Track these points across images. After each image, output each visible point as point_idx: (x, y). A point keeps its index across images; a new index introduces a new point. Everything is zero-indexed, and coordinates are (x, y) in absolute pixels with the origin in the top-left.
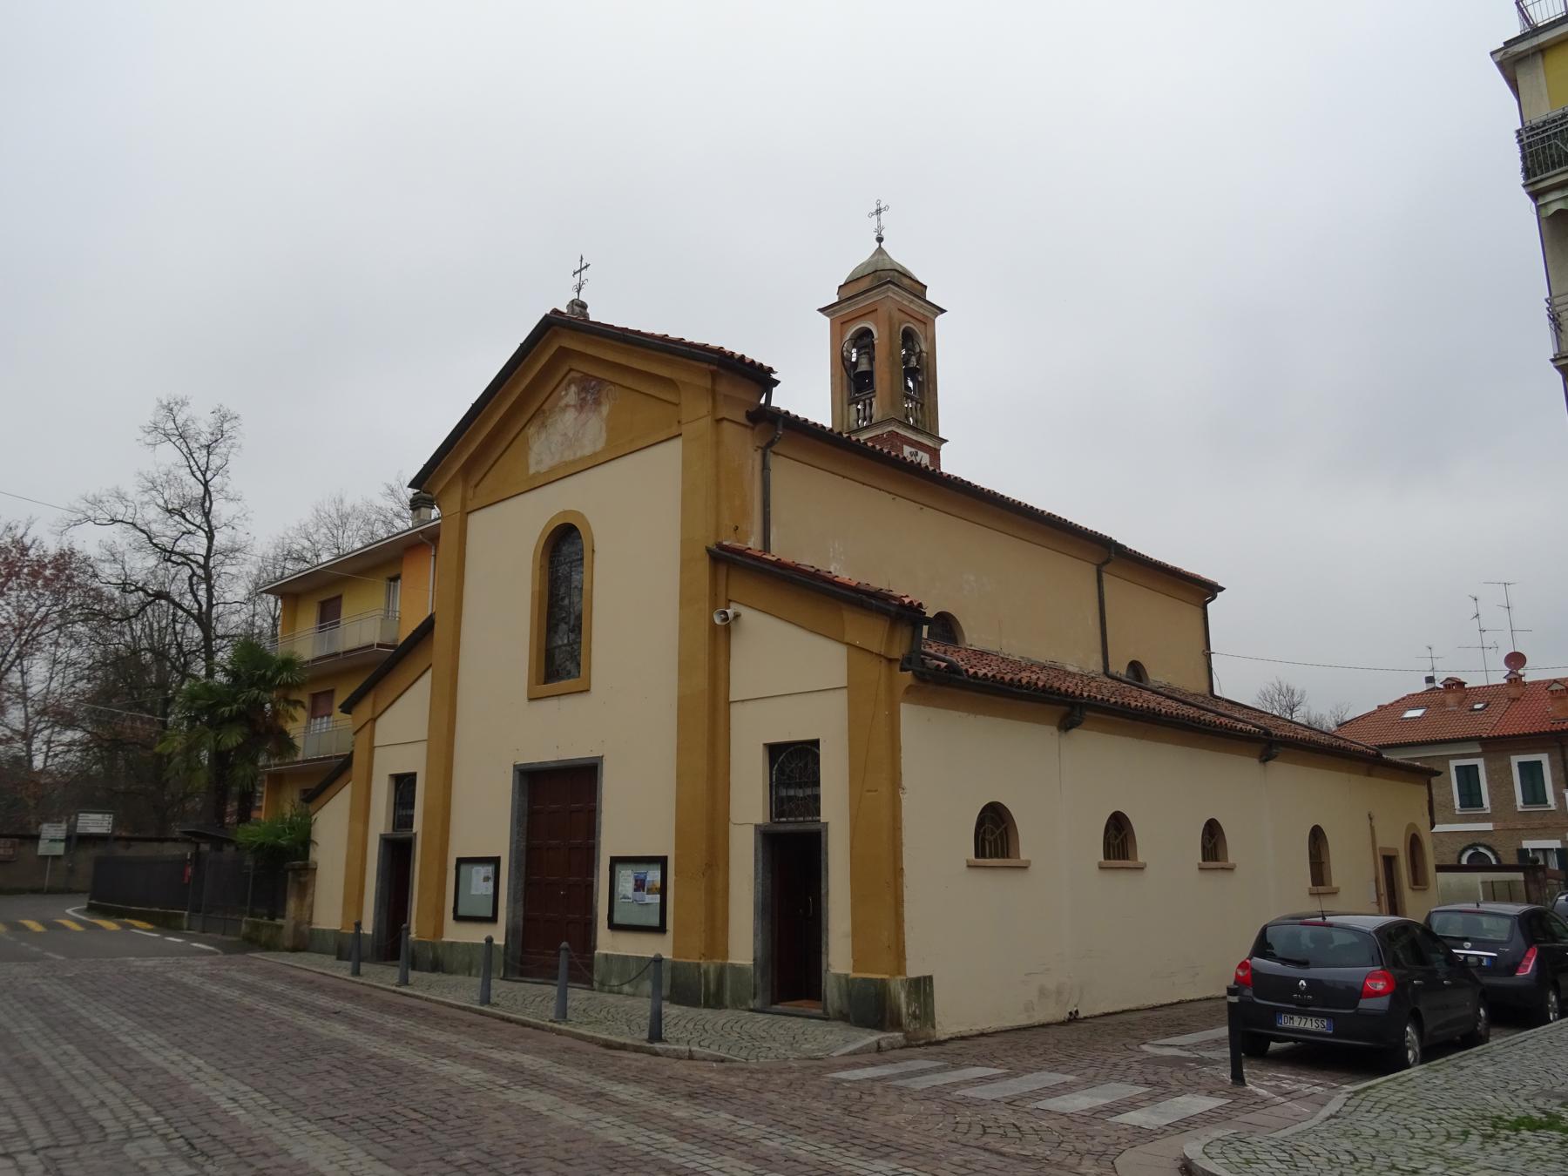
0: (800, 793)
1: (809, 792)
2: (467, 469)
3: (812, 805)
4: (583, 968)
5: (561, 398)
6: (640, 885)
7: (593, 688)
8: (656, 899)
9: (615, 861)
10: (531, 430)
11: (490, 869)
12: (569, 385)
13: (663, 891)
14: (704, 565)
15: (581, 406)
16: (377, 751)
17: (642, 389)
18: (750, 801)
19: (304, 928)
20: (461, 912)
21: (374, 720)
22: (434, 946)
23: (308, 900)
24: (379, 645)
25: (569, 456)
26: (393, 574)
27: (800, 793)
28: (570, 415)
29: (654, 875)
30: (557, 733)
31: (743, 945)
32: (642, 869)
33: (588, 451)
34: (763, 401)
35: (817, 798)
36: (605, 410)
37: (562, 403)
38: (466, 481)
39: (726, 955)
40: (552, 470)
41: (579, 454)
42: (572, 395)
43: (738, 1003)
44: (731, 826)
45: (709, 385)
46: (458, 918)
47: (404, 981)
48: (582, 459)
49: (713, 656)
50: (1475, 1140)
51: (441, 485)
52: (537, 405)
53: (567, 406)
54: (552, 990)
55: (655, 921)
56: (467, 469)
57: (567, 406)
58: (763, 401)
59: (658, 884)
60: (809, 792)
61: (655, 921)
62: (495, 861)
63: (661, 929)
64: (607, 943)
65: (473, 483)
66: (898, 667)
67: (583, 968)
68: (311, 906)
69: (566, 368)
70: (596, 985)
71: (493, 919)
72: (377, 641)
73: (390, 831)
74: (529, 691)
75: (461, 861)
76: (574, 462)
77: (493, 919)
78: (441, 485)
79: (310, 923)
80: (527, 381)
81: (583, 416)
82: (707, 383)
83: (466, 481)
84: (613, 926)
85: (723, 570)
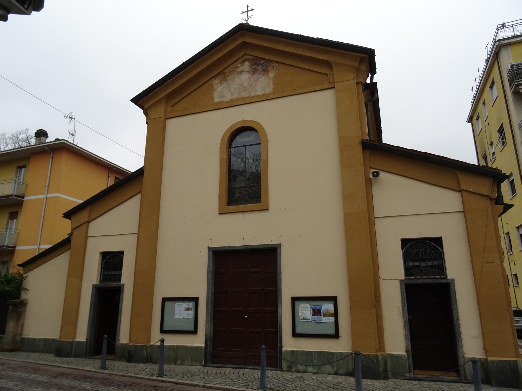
0: (423, 264)
1: (117, 273)
2: (169, 97)
3: (118, 278)
4: (275, 359)
5: (237, 67)
6: (317, 312)
7: (271, 208)
8: (332, 319)
9: (295, 300)
10: (215, 81)
11: (191, 304)
12: (244, 61)
13: (336, 314)
14: (358, 151)
15: (254, 72)
16: (89, 240)
18: (392, 269)
19: (18, 338)
20: (166, 328)
21: (89, 222)
22: (147, 348)
23: (21, 321)
24: (16, 196)
26: (20, 165)
27: (423, 264)
28: (245, 77)
29: (328, 307)
30: (244, 230)
31: (396, 341)
32: (317, 304)
33: (260, 93)
34: (368, 81)
35: (120, 275)
36: (272, 75)
37: (239, 70)
38: (167, 103)
39: (384, 351)
40: (231, 101)
41: (253, 94)
42: (246, 66)
43: (397, 375)
44: (381, 281)
45: (357, 65)
46: (295, 335)
47: (103, 367)
48: (257, 96)
49: (367, 195)
50: (197, 371)
51: (150, 103)
52: (221, 69)
53: (242, 71)
54: (257, 373)
55: (332, 332)
56: (169, 97)
57: (242, 71)
58: (368, 81)
60: (117, 273)
61: (332, 332)
62: (196, 300)
63: (336, 336)
64: (289, 344)
65: (172, 104)
66: (494, 202)
67: (275, 359)
68: (22, 326)
69: (244, 53)
70: (285, 365)
71: (195, 332)
72: (15, 193)
73: (98, 283)
74: (220, 209)
75: (165, 300)
77: (195, 332)
79: (21, 335)
80: (219, 56)
81: (255, 77)
82: (357, 65)
83: (167, 103)
84: (295, 335)
85: (368, 153)
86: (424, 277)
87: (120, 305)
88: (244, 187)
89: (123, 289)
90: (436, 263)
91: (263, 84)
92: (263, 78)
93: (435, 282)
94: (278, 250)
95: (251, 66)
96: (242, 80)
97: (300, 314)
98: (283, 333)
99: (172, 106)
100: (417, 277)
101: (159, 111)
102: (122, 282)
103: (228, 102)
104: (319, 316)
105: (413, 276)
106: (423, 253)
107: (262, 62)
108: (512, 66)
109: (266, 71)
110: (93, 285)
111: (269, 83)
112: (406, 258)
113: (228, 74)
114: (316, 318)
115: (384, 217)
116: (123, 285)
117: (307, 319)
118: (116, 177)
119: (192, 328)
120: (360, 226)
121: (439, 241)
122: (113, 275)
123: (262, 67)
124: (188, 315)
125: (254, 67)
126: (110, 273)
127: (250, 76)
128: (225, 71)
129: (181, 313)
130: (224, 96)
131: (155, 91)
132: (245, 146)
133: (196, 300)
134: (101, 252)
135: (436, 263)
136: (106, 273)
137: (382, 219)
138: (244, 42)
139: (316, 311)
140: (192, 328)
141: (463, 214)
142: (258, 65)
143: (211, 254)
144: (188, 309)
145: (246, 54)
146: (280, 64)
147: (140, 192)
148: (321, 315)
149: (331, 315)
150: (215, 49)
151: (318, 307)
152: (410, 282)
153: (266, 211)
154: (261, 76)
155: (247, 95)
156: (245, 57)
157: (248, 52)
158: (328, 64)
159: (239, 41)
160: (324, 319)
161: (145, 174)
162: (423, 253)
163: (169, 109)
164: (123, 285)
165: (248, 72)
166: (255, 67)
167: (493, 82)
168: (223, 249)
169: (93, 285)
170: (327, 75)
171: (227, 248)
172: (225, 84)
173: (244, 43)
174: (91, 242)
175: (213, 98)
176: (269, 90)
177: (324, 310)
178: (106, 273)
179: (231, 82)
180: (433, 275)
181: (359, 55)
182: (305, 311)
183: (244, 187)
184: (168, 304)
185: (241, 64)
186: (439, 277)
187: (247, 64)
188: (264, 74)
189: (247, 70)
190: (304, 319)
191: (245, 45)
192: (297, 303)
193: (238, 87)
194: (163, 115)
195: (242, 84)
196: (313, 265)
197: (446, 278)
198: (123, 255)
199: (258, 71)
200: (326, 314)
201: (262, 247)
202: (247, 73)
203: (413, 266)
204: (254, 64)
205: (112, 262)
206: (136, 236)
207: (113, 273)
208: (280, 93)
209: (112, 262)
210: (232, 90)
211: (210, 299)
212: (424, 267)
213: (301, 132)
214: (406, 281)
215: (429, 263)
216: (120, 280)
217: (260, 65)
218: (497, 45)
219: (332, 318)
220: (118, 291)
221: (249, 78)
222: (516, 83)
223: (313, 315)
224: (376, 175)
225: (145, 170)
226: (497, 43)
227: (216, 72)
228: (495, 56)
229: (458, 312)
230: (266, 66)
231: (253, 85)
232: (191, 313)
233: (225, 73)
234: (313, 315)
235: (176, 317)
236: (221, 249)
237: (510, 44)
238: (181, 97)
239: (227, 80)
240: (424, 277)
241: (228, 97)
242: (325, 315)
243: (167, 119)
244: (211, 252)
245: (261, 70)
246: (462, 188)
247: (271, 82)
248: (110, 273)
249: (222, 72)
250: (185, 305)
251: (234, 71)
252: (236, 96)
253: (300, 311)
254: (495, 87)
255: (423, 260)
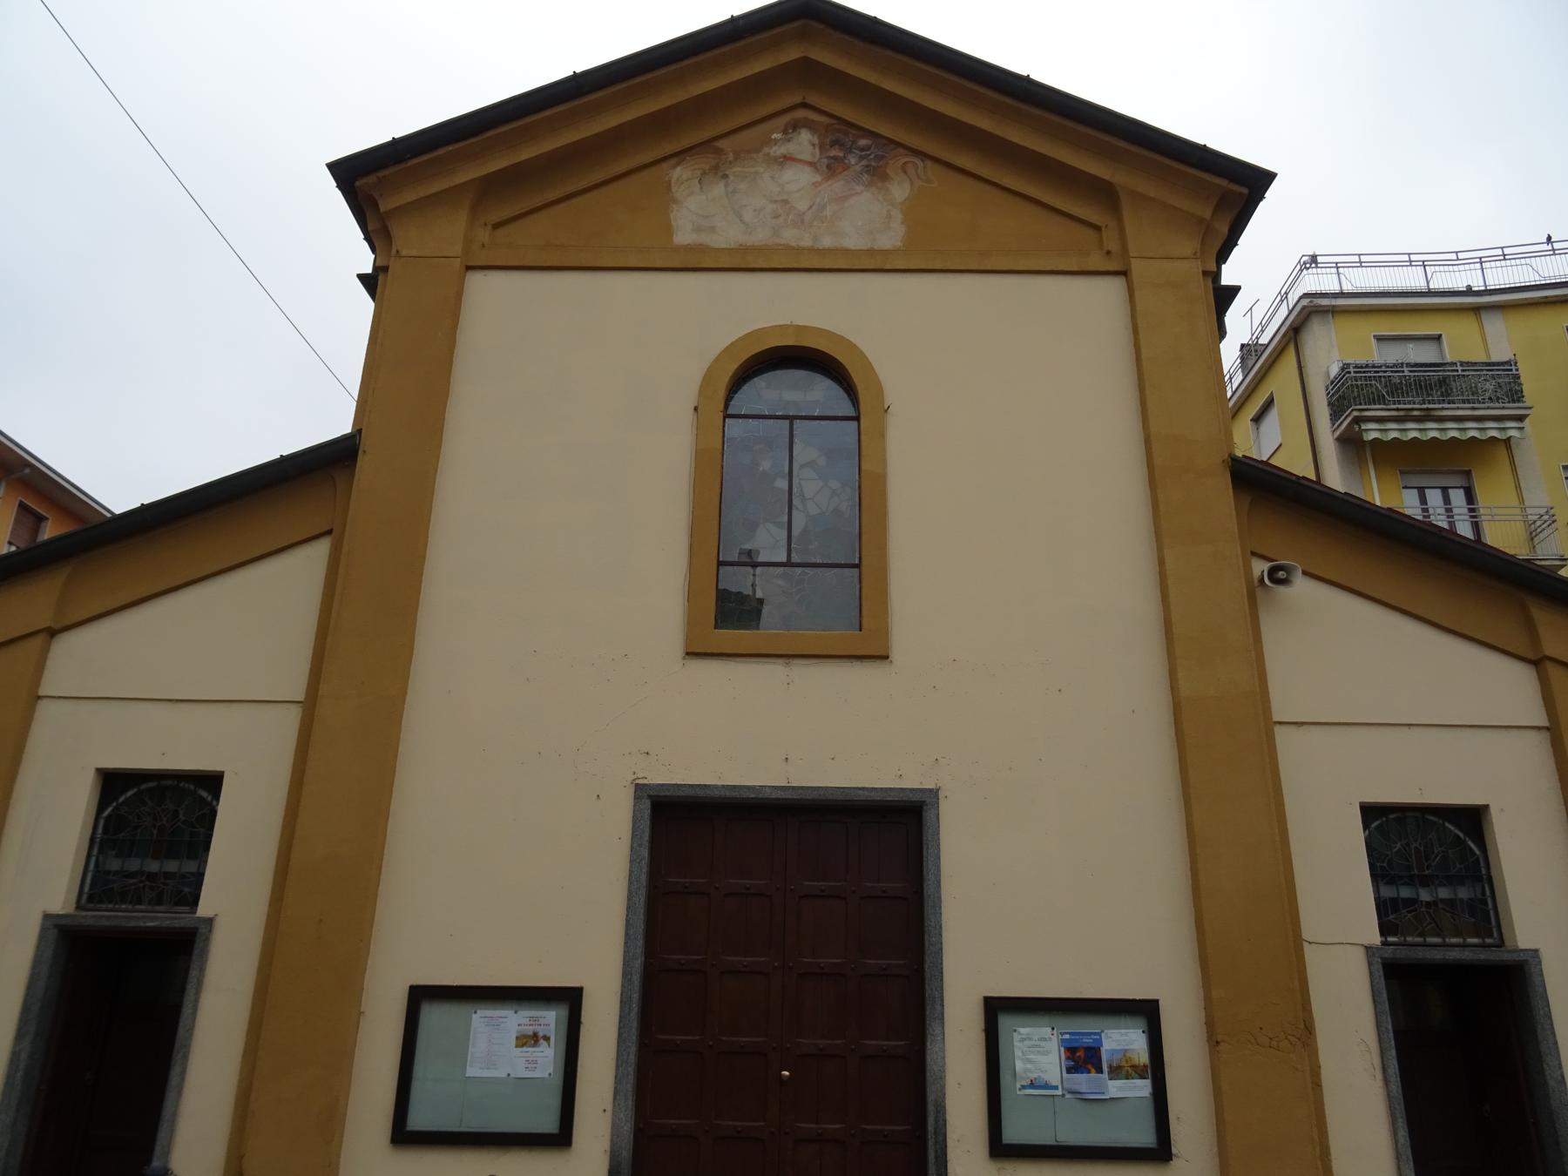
0: (1425, 895)
5: (770, 142)
6: (1083, 1058)
7: (896, 653)
10: (679, 172)
11: (550, 1019)
12: (795, 126)
13: (1156, 1069)
15: (833, 168)
16: (45, 710)
17: (1008, 181)
18: (1339, 909)
20: (419, 1120)
21: (52, 633)
25: (790, 236)
27: (1425, 895)
28: (798, 180)
29: (1125, 1039)
30: (781, 732)
32: (1084, 1026)
35: (199, 877)
36: (900, 190)
40: (744, 250)
41: (827, 242)
42: (804, 143)
51: (409, 196)
55: (1144, 1136)
57: (787, 159)
59: (1143, 1057)
61: (1144, 1136)
62: (570, 998)
69: (797, 99)
76: (799, 250)
78: (409, 196)
81: (838, 186)
82: (1207, 214)
86: (1431, 940)
87: (186, 1011)
88: (782, 566)
89: (207, 940)
90: (1463, 893)
91: (868, 213)
92: (867, 195)
93: (1482, 957)
94: (928, 815)
95: (822, 147)
96: (781, 186)
97: (1019, 1065)
98: (950, 1143)
99: (496, 226)
100: (1409, 939)
101: (445, 233)
102: (203, 910)
103: (730, 251)
104: (1093, 1075)
105: (1395, 934)
106: (1433, 855)
107: (863, 142)
108: (1345, 368)
109: (876, 174)
110: (47, 917)
111: (889, 216)
112: (1381, 872)
113: (731, 157)
114: (1082, 1081)
115: (1303, 724)
116: (209, 922)
117: (1047, 1086)
118: (22, 506)
119: (548, 1123)
120: (1223, 748)
121: (1473, 819)
122: (152, 877)
123: (862, 158)
124: (532, 1064)
125: (832, 154)
126: (134, 865)
127: (818, 178)
128: (720, 144)
129: (499, 1057)
130: (713, 229)
131: (441, 151)
132: (791, 419)
133: (570, 998)
134: (99, 771)
135: (1463, 893)
136: (114, 865)
137: (1293, 728)
138: (805, 58)
139: (1080, 1054)
140: (550, 1125)
141: (1545, 736)
142: (850, 151)
143: (647, 813)
144: (530, 1039)
145: (804, 105)
146: (929, 163)
147: (329, 532)
148: (1100, 1070)
149: (1140, 1072)
150: (701, 57)
151: (1088, 1041)
152: (1403, 954)
153: (878, 663)
154: (859, 188)
155: (807, 242)
156: (801, 114)
157: (813, 99)
158: (1106, 195)
159: (791, 54)
160: (1115, 1088)
161: (363, 462)
162: (1433, 855)
163: (483, 235)
164: (209, 922)
165: (811, 164)
166: (835, 152)
167: (1269, 404)
168: (701, 793)
169: (47, 917)
170: (1097, 228)
171: (717, 793)
172: (718, 189)
173: (806, 65)
174: (49, 723)
175: (668, 230)
176: (891, 238)
177: (1113, 1052)
178: (114, 865)
179: (743, 186)
180: (1422, 935)
181: (1224, 183)
182: (1036, 1052)
183: (782, 566)
184: (434, 1016)
185: (785, 132)
186: (1460, 940)
187: (805, 136)
188: (869, 185)
189: (808, 157)
190: (1032, 1085)
191: (807, 72)
192: (1005, 1022)
193: (770, 207)
194: (457, 249)
195: (786, 202)
196: (1057, 884)
197: (1501, 943)
198: (216, 795)
199: (846, 168)
200: (1119, 1067)
201: (863, 796)
202: (808, 169)
203: (1392, 900)
204: (834, 143)
205: (156, 818)
206: (293, 716)
207: (153, 866)
208: (923, 256)
209: (156, 818)
210: (748, 216)
211: (636, 996)
212: (1428, 904)
213: (998, 400)
214: (1389, 952)
215: (1444, 893)
216: (194, 900)
217: (852, 148)
218: (1304, 308)
219: (1140, 1082)
220: (181, 950)
221: (815, 185)
222: (1356, 414)
223: (1069, 1071)
224: (1279, 576)
225: (366, 443)
226: (1305, 302)
227: (686, 143)
228: (1291, 334)
229: (1560, 1067)
230: (879, 158)
231: (828, 212)
232: (547, 1060)
233: (718, 152)
234: (1069, 1071)
235: (471, 1072)
236: (691, 793)
237: (1333, 311)
238: (537, 201)
239: (725, 176)
240: (1431, 940)
241: (728, 235)
242: (1116, 1072)
243: (469, 268)
244: (647, 804)
245: (858, 168)
246: (1549, 652)
247: (898, 216)
248: (134, 865)
249: (706, 146)
250: (514, 1019)
251: (758, 151)
252: (760, 237)
253: (1018, 1053)
254: (1272, 418)
255: (1425, 882)
